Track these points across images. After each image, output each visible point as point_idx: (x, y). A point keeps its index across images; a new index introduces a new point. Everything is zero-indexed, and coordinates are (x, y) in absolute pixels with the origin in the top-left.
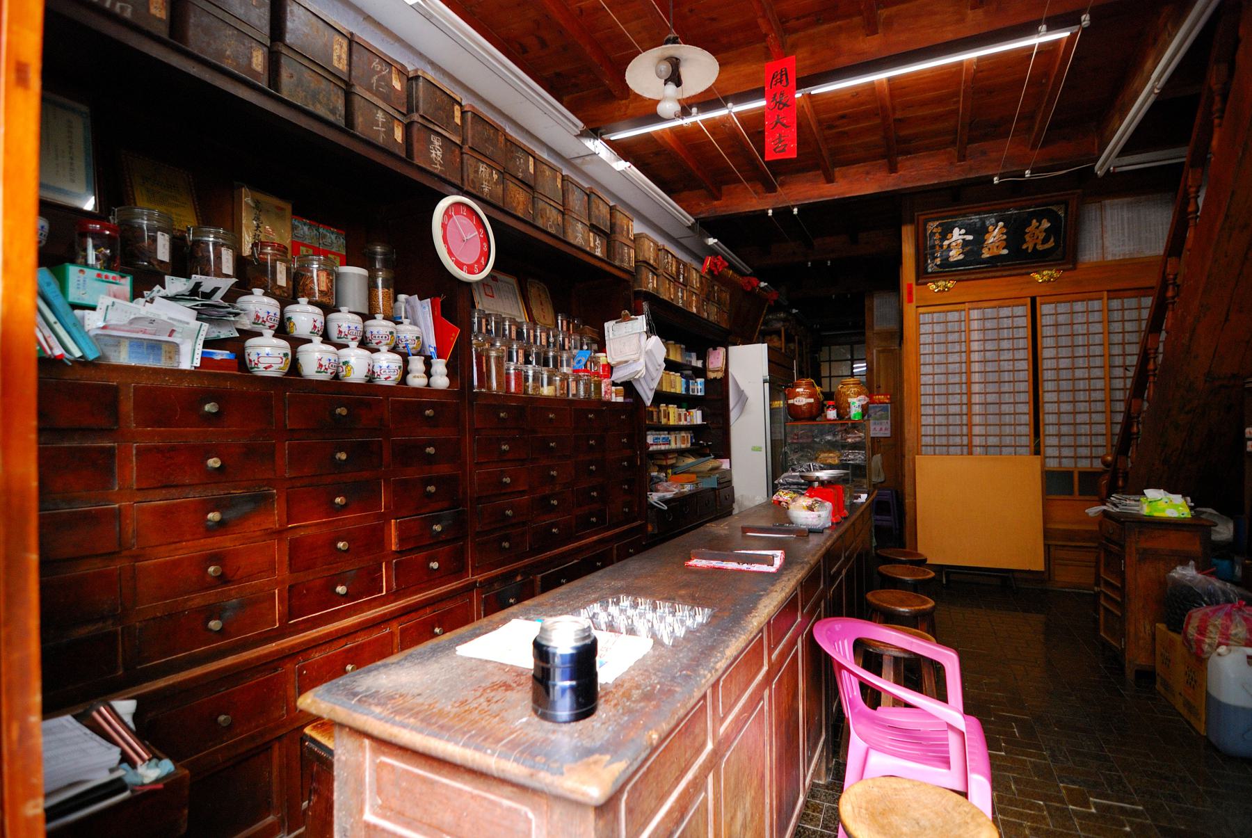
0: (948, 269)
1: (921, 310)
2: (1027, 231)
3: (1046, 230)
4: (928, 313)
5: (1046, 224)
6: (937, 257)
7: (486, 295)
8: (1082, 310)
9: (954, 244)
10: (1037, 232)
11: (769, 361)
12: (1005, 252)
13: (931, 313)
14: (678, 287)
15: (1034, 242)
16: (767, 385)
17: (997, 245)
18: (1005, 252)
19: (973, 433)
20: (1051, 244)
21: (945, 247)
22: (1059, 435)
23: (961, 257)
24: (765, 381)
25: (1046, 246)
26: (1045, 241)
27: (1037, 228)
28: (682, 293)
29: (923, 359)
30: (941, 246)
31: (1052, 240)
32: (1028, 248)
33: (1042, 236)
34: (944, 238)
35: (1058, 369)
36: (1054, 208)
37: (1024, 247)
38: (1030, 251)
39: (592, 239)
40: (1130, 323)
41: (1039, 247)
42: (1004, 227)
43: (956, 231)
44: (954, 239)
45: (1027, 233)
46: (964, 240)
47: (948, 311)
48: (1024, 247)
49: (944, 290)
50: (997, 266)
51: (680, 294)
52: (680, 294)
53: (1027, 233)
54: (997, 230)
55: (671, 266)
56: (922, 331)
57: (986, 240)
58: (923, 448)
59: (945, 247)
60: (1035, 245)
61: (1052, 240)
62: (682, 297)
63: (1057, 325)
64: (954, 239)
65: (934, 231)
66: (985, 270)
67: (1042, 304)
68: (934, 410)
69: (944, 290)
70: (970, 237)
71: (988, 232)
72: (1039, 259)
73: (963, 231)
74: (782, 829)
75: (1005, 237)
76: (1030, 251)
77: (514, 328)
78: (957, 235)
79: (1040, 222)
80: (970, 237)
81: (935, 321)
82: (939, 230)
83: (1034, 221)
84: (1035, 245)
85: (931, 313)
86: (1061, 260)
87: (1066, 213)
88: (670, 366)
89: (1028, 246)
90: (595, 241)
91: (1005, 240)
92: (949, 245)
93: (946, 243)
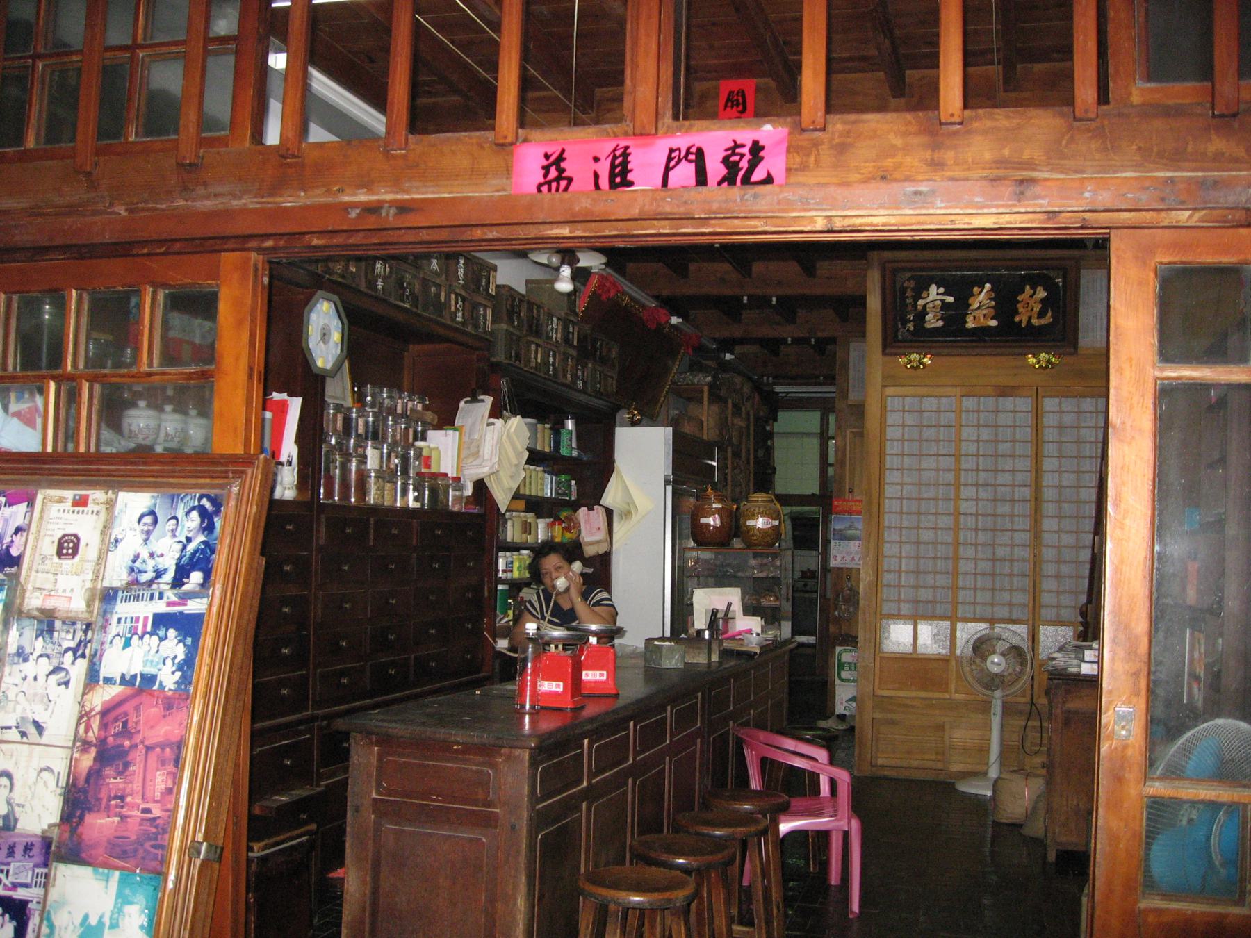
0: (922, 338)
1: (889, 391)
2: (1019, 298)
3: (1042, 301)
4: (898, 396)
5: (1041, 294)
6: (909, 321)
7: (842, 680)
8: (1091, 409)
9: (931, 305)
10: (1031, 302)
11: (674, 451)
12: (994, 323)
13: (901, 396)
14: (550, 350)
15: (1029, 314)
16: (669, 488)
17: (984, 312)
18: (994, 323)
19: (661, 635)
20: (1048, 319)
21: (920, 308)
22: (1058, 577)
23: (940, 324)
24: (667, 482)
25: (1043, 322)
26: (1041, 315)
27: (1031, 296)
28: (554, 358)
29: (889, 461)
30: (915, 306)
31: (1049, 314)
32: (1021, 321)
33: (1037, 308)
34: (918, 297)
35: (1060, 487)
36: (1052, 274)
37: (1017, 319)
38: (1023, 325)
39: (453, 302)
40: (944, 518)
41: (1035, 322)
42: (992, 290)
43: (933, 289)
44: (931, 298)
45: (1019, 302)
46: (943, 301)
47: (923, 396)
48: (1017, 319)
49: (918, 367)
50: (985, 341)
51: (551, 360)
52: (551, 360)
53: (1019, 302)
54: (983, 294)
55: (556, 333)
56: (889, 421)
57: (970, 305)
58: (885, 590)
59: (920, 308)
60: (1030, 318)
61: (1049, 314)
62: (554, 363)
63: (1060, 427)
64: (931, 298)
65: (906, 284)
66: (969, 344)
67: (1043, 397)
68: (901, 535)
69: (918, 367)
70: (950, 299)
71: (973, 295)
72: (1031, 337)
73: (942, 290)
74: (701, 935)
75: (993, 303)
76: (1023, 325)
77: (340, 417)
78: (934, 294)
79: (1034, 288)
80: (950, 299)
81: (906, 408)
82: (912, 284)
83: (1028, 287)
84: (1030, 318)
85: (901, 396)
86: (1059, 341)
87: (1064, 281)
88: (535, 458)
89: (1022, 318)
90: (456, 303)
91: (992, 307)
92: (925, 306)
93: (921, 302)
